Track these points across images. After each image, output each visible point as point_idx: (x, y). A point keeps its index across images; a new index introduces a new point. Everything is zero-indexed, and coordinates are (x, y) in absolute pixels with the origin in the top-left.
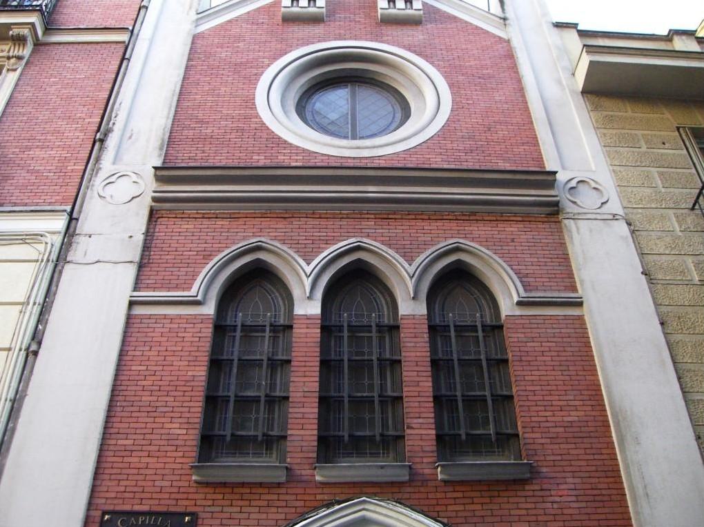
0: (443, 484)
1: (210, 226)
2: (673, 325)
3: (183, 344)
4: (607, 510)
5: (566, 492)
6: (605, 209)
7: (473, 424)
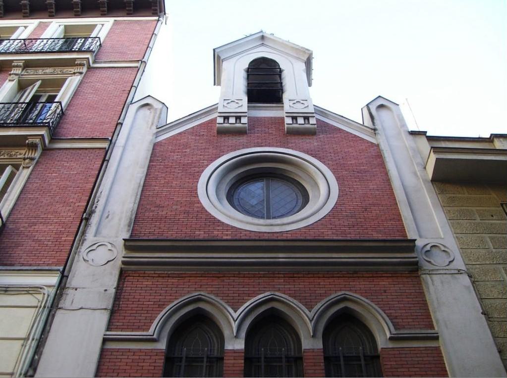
6: (452, 266)
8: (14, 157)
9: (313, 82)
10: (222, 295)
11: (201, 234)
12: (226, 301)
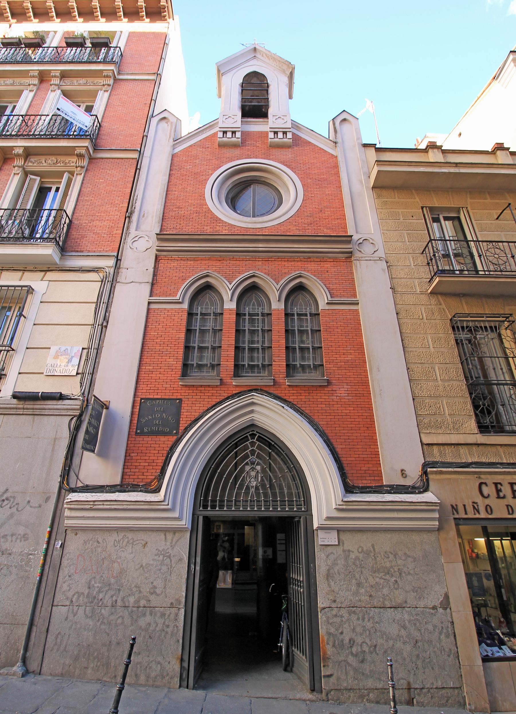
0: (288, 387)
1: (185, 264)
2: (403, 314)
3: (174, 322)
4: (361, 400)
5: (343, 392)
6: (376, 254)
7: (303, 358)
8: (68, 165)
9: (294, 95)
10: (222, 273)
11: (208, 230)
12: (225, 277)
